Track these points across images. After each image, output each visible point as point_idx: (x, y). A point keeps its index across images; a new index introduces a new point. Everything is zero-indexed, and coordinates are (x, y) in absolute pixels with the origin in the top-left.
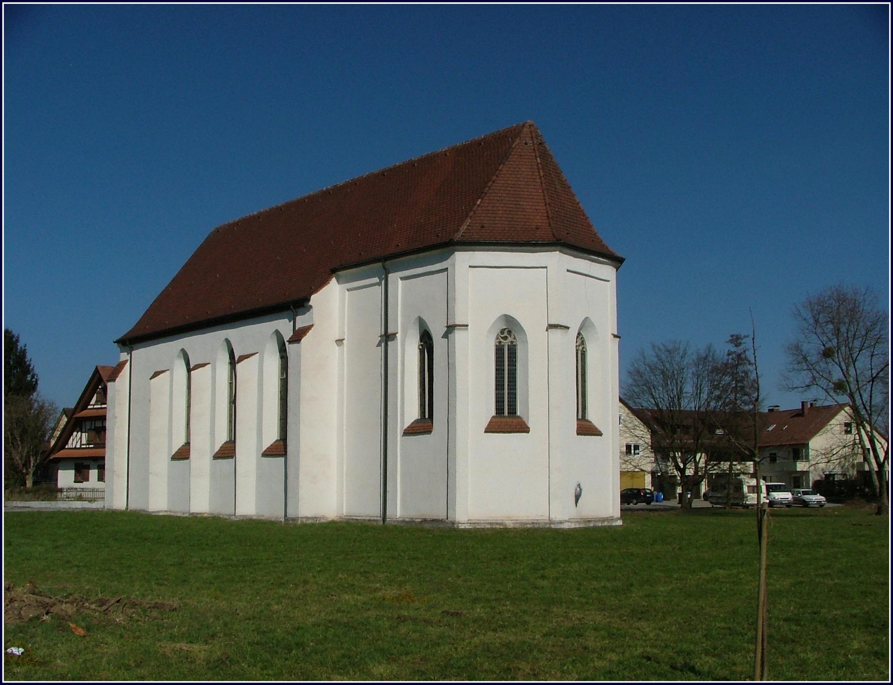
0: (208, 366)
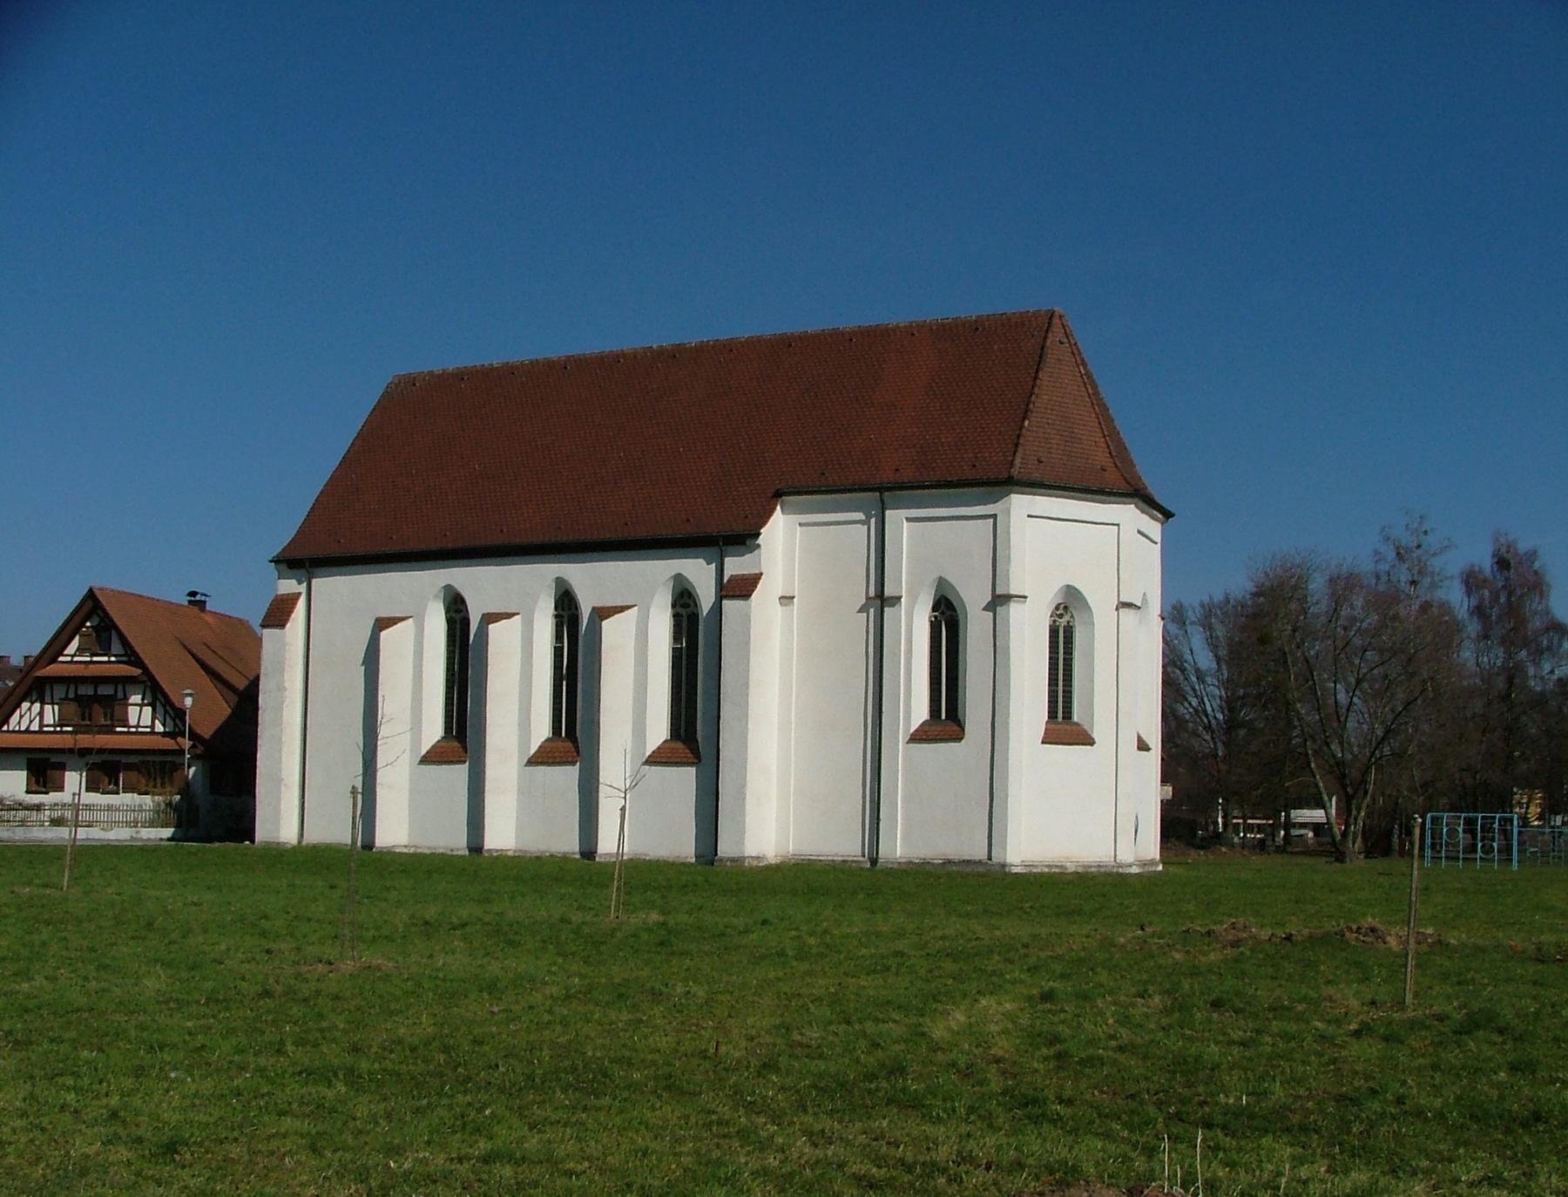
0: (516, 617)
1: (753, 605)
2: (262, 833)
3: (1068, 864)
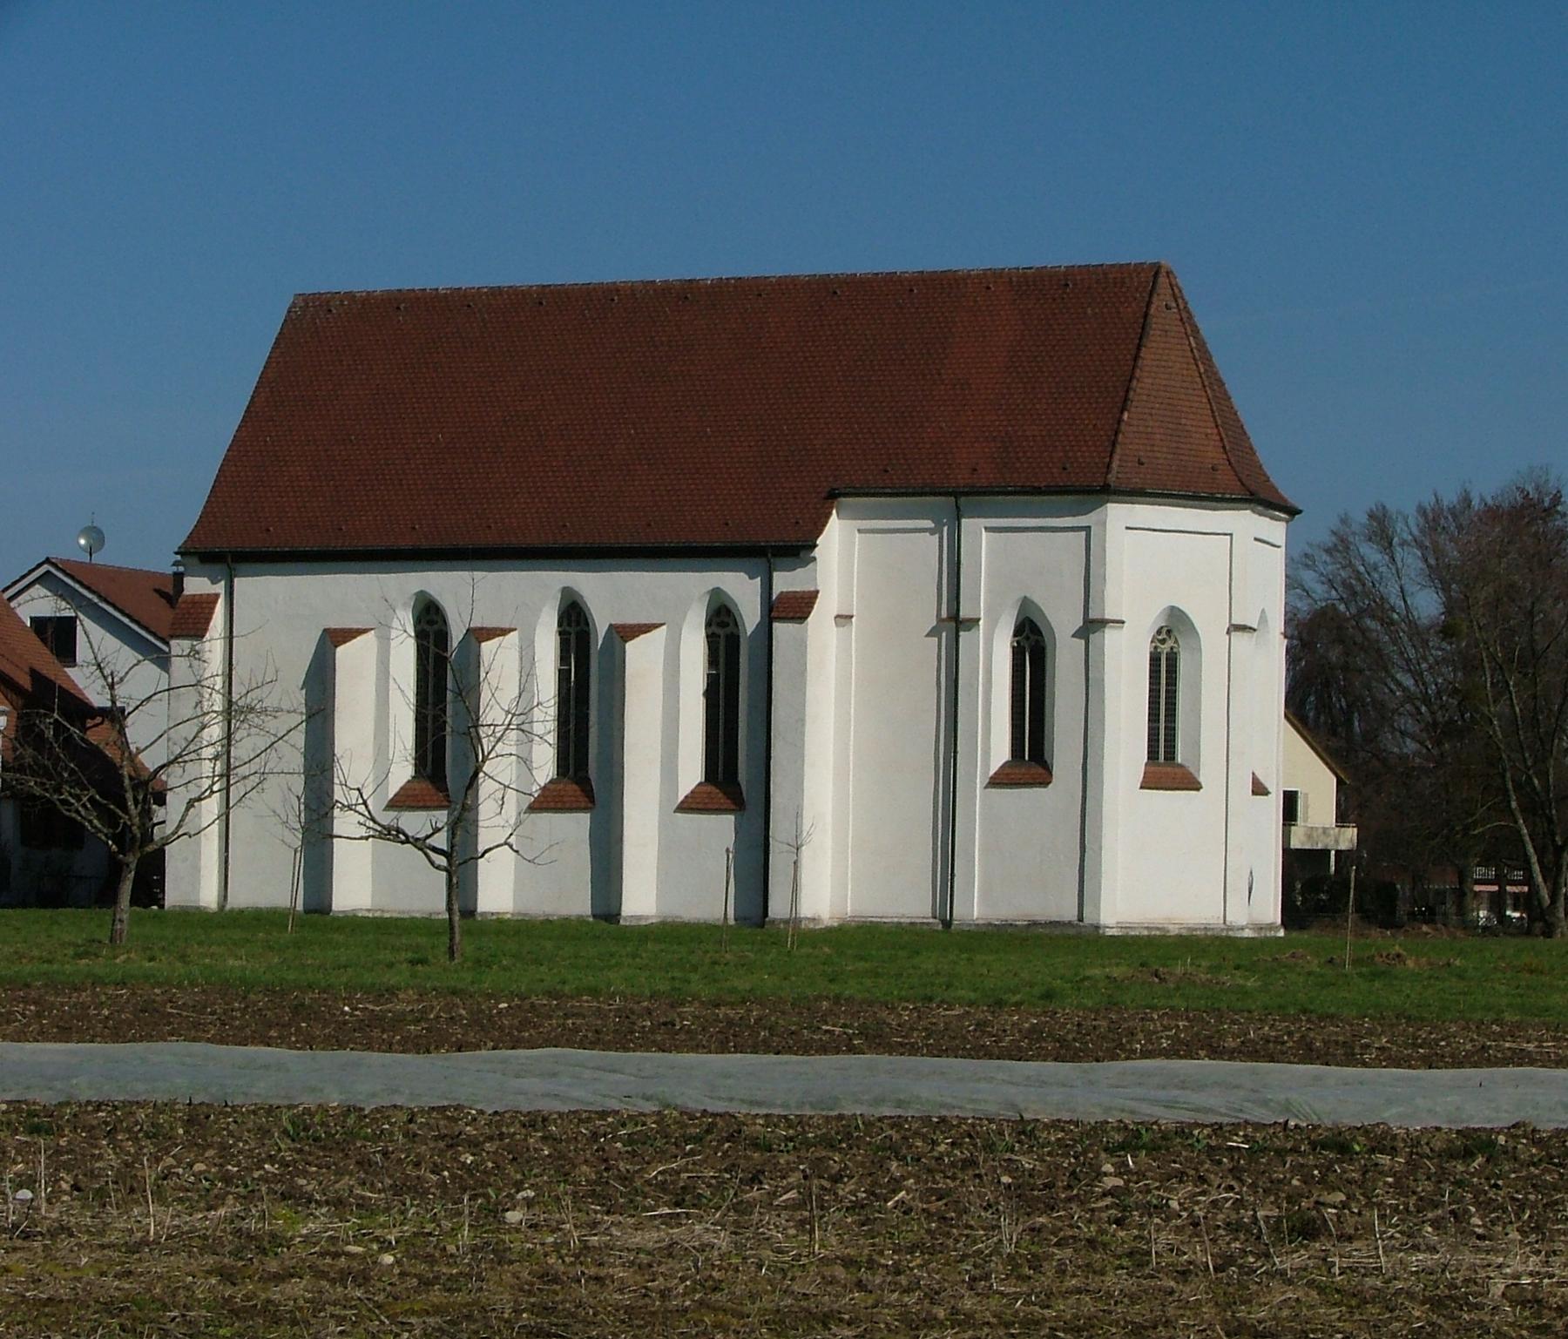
1: (809, 628)
2: (174, 895)
3: (1171, 927)
